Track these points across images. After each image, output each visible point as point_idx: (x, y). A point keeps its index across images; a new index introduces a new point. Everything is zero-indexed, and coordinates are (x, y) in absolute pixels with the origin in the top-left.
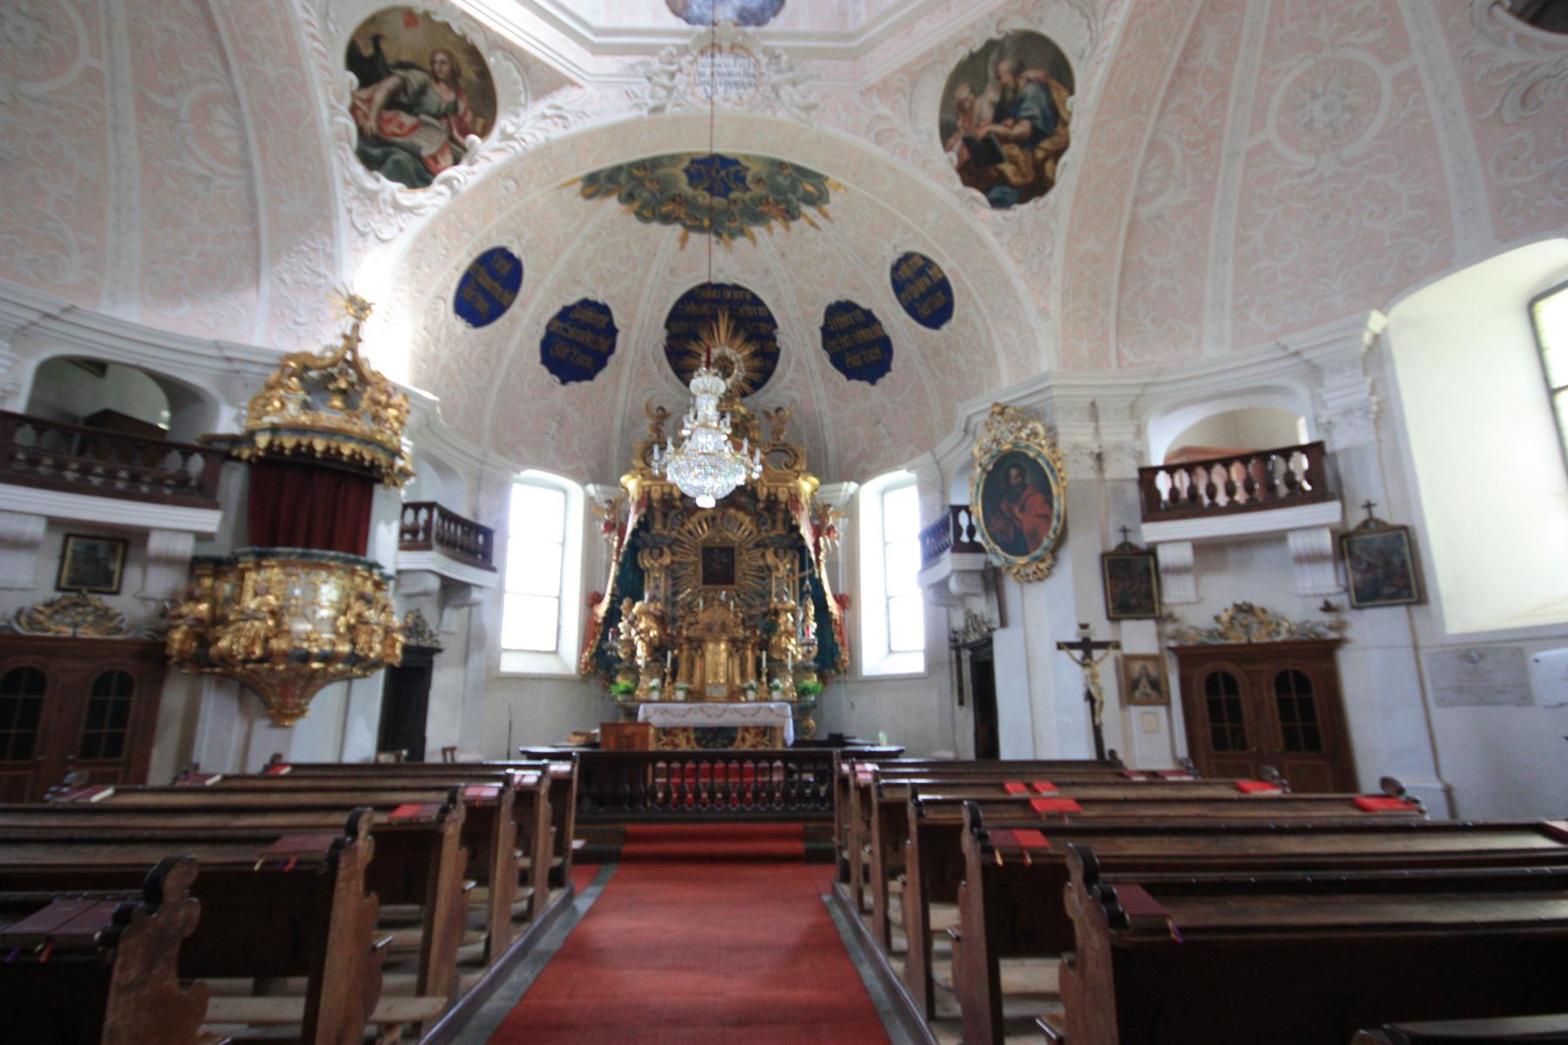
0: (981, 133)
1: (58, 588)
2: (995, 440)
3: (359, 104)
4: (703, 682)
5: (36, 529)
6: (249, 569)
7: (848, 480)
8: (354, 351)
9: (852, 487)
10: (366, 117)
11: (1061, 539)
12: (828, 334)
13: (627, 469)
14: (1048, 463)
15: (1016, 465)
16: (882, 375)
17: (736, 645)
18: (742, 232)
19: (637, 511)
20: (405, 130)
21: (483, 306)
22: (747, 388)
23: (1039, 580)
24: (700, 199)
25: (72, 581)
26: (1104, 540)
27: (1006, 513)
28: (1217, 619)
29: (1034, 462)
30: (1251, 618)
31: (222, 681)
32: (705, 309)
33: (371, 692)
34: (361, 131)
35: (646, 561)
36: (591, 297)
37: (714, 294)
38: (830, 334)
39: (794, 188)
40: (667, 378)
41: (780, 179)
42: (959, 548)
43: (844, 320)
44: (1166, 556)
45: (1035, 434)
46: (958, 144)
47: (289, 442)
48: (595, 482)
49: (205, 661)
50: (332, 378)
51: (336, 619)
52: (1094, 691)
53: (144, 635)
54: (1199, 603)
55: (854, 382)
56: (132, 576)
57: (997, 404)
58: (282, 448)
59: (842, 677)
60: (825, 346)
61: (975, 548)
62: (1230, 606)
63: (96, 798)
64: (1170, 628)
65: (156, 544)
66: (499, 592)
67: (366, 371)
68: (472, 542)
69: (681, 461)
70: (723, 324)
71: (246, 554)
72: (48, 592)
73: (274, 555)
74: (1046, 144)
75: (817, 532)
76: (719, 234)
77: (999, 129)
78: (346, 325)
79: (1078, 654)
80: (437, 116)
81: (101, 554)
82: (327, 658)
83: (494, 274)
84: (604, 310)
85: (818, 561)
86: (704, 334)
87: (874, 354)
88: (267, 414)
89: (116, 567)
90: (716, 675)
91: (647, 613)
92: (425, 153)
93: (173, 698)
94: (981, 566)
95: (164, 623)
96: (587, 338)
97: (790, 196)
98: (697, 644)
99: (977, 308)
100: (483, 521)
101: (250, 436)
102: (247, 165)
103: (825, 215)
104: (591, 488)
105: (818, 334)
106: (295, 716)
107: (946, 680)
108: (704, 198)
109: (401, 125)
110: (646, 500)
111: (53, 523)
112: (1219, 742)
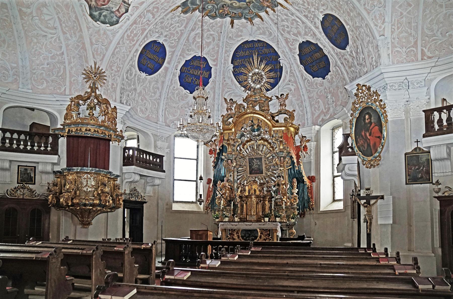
1: (18, 183)
15: (368, 113)
20: (106, 2)
22: (269, 87)
25: (21, 181)
43: (307, 50)
49: (58, 206)
63: (37, 244)
68: (154, 162)
70: (255, 57)
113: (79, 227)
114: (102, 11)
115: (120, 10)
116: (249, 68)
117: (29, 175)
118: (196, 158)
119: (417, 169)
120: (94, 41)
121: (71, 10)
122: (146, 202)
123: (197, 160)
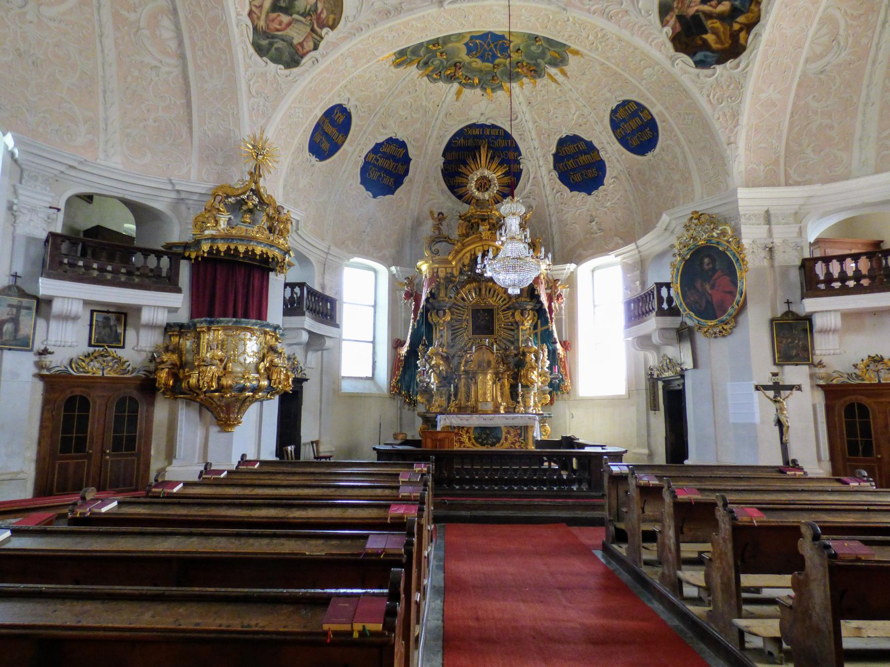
0: (691, 11)
1: (90, 345)
2: (693, 238)
3: (254, 9)
4: (477, 401)
5: (77, 308)
6: (203, 332)
7: (571, 263)
8: (256, 183)
9: (571, 267)
10: (259, 18)
11: (743, 308)
12: (558, 158)
13: (422, 257)
14: (734, 255)
15: (708, 256)
17: (498, 377)
18: (501, 87)
19: (429, 286)
20: (283, 26)
21: (325, 146)
23: (724, 336)
24: (474, 65)
25: (98, 341)
26: (774, 309)
27: (699, 287)
28: (855, 366)
29: (723, 254)
30: (880, 367)
31: (189, 401)
32: (470, 142)
33: (272, 406)
34: (255, 29)
35: (433, 318)
37: (477, 132)
39: (543, 55)
40: (443, 192)
41: (533, 48)
42: (661, 313)
43: (570, 149)
44: (819, 322)
45: (724, 233)
46: (672, 20)
47: (223, 247)
48: (396, 264)
50: (242, 202)
51: (257, 365)
52: (783, 419)
53: (142, 374)
55: (575, 193)
56: (131, 335)
57: (696, 212)
58: (218, 249)
59: (566, 396)
61: (674, 312)
62: (865, 357)
65: (146, 316)
66: (339, 340)
68: (324, 307)
69: (497, 265)
70: (483, 152)
71: (201, 323)
72: (83, 348)
73: (218, 322)
74: (741, 19)
75: (550, 299)
76: (484, 89)
77: (706, 8)
78: (250, 166)
79: (771, 394)
80: (304, 15)
81: (112, 323)
82: (255, 390)
83: (333, 123)
84: (403, 145)
85: (551, 319)
87: (592, 173)
88: (208, 228)
89: (120, 330)
90: (485, 394)
91: (437, 354)
92: (295, 42)
93: (161, 411)
94: (678, 326)
95: (152, 367)
96: (389, 164)
97: (539, 61)
98: (471, 376)
99: (678, 142)
100: (328, 293)
101: (197, 243)
102: (182, 57)
103: (564, 73)
104: (393, 269)
105: (551, 159)
106: (234, 425)
107: (643, 399)
108: (478, 63)
109: (281, 23)
110: (434, 276)
111: (86, 303)
112: (853, 449)
113: (214, 430)
114: (275, 40)
115: (305, 44)
116: (473, 166)
117: (114, 328)
119: (791, 343)
120: (254, 93)
121: (220, 30)
122: (306, 380)
123: (375, 306)
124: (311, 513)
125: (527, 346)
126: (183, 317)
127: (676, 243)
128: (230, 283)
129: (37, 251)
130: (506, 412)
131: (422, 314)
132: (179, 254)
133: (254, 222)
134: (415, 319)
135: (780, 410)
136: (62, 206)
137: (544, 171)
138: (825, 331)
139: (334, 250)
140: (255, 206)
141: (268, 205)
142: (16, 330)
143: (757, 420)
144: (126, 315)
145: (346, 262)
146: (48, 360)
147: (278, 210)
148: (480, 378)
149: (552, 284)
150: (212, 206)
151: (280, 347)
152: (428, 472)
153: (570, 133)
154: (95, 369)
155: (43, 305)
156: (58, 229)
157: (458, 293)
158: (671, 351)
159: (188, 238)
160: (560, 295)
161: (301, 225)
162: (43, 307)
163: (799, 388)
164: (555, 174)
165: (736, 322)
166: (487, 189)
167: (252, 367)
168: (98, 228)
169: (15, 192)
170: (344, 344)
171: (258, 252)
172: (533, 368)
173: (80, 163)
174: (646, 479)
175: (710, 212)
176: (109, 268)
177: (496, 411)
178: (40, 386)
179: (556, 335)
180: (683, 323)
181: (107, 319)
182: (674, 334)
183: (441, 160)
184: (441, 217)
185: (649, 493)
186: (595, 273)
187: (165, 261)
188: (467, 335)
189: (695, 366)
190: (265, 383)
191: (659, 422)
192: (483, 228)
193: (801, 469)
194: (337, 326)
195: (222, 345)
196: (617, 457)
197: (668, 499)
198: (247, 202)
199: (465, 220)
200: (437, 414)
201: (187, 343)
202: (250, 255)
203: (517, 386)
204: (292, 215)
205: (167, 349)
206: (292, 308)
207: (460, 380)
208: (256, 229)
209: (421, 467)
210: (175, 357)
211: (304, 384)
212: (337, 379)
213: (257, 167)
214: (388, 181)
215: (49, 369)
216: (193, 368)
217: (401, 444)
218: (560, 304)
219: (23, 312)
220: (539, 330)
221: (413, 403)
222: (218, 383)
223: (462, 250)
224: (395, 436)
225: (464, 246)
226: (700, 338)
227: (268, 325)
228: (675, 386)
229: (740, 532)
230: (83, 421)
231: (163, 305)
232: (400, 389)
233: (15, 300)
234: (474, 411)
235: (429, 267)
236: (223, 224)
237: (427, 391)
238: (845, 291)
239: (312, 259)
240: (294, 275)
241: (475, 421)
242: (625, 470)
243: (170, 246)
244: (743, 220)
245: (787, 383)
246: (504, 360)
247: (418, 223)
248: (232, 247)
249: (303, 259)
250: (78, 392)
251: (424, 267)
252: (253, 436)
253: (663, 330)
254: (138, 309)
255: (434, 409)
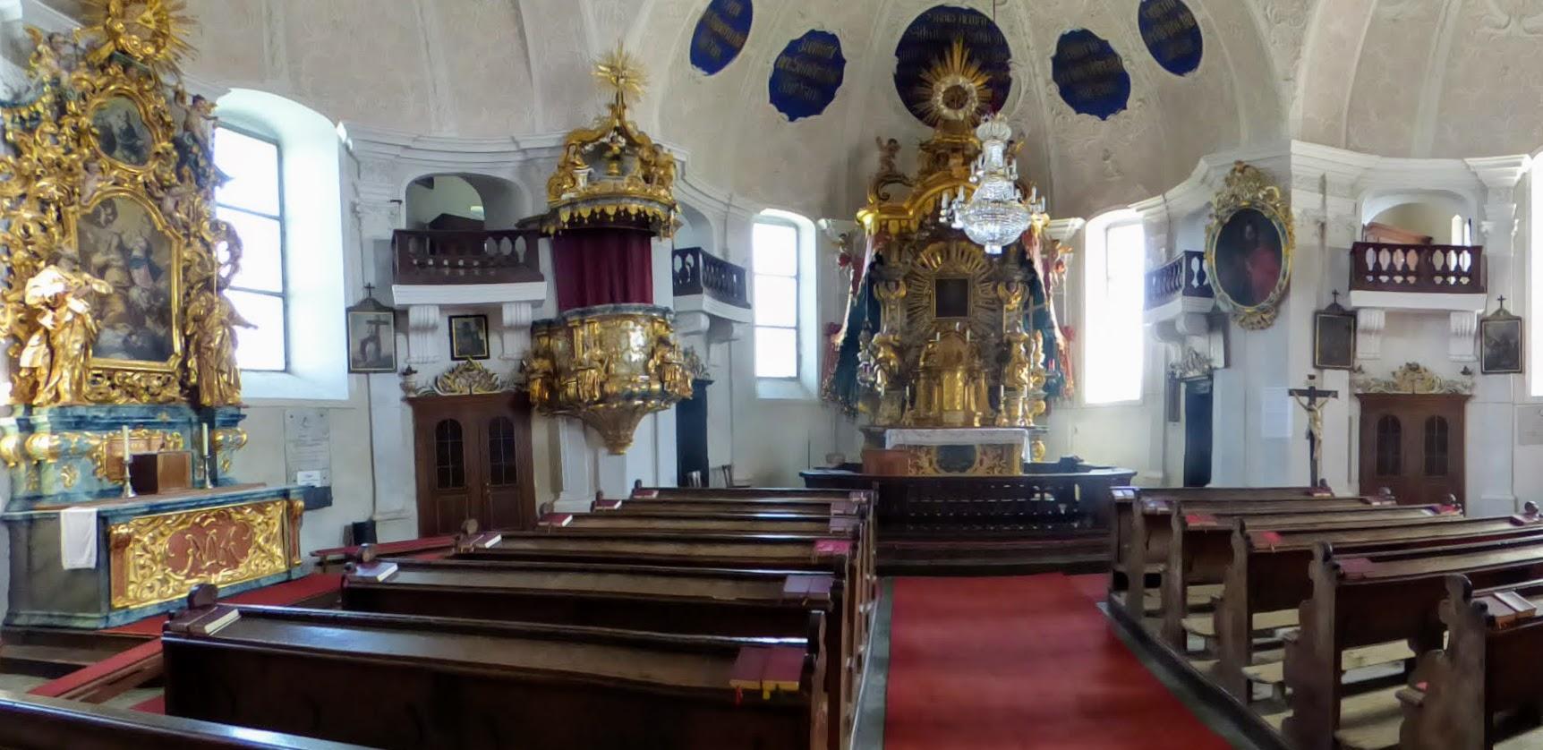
1: (453, 358)
4: (941, 409)
5: (434, 316)
8: (620, 117)
9: (1076, 223)
11: (1285, 293)
13: (863, 204)
16: (1113, 111)
17: (971, 376)
25: (460, 352)
29: (1268, 222)
33: (669, 417)
35: (880, 292)
36: (818, 28)
38: (1061, 65)
42: (1189, 291)
43: (1076, 50)
44: (1363, 319)
45: (1270, 195)
47: (585, 212)
50: (606, 147)
51: (646, 363)
52: (1316, 432)
53: (512, 388)
54: (1380, 358)
56: (494, 341)
57: (1239, 162)
60: (1056, 77)
61: (1206, 292)
64: (1360, 378)
65: (508, 316)
66: (751, 326)
67: (635, 134)
75: (1047, 269)
79: (1305, 400)
82: (646, 396)
84: (832, 40)
86: (935, 62)
88: (564, 191)
89: (482, 336)
90: (953, 400)
91: (885, 343)
93: (539, 432)
94: (1208, 309)
95: (522, 378)
96: (812, 70)
98: (934, 375)
101: (555, 212)
104: (823, 222)
105: (1050, 64)
106: (624, 445)
107: (1160, 406)
111: (443, 308)
113: (603, 452)
118: (279, 290)
123: (798, 277)
124: (720, 551)
125: (1014, 333)
126: (550, 311)
127: (1214, 200)
128: (603, 255)
129: (387, 254)
130: (983, 426)
131: (864, 287)
132: (535, 231)
133: (623, 172)
134: (854, 293)
135: (1314, 420)
136: (403, 197)
137: (1040, 80)
138: (1368, 331)
139: (738, 201)
140: (622, 149)
141: (640, 146)
142: (378, 349)
143: (1290, 435)
144: (485, 317)
145: (756, 216)
146: (414, 378)
147: (655, 150)
148: (946, 377)
149: (1050, 246)
150: (566, 161)
151: (671, 337)
152: (869, 502)
153: (1077, 27)
154: (461, 387)
155: (400, 316)
156: (403, 226)
157: (916, 257)
158: (1199, 343)
159: (543, 209)
160: (1060, 263)
161: (688, 166)
162: (401, 319)
163: (1335, 394)
164: (1054, 88)
165: (1277, 312)
166: (962, 106)
167: (640, 366)
168: (444, 216)
169: (357, 193)
170: (759, 333)
171: (633, 211)
172: (1022, 364)
173: (415, 140)
174: (1154, 505)
175: (1256, 165)
176: (461, 263)
177: (968, 423)
178: (409, 410)
179: (1054, 318)
180: (1216, 308)
181: (466, 325)
182: (1203, 322)
183: (894, 62)
184: (892, 147)
185: (1157, 522)
186: (1111, 232)
187: (521, 243)
188: (928, 317)
189: (1227, 364)
190: (656, 387)
191: (1178, 436)
192: (955, 162)
193: (1328, 490)
194: (748, 306)
195: (600, 341)
196: (1124, 480)
197: (1176, 527)
198: (611, 146)
199: (927, 150)
200: (886, 427)
201: (559, 345)
202: (623, 216)
203: (998, 389)
204: (676, 156)
205: (536, 355)
206: (685, 283)
207: (918, 379)
208: (626, 180)
209: (859, 497)
210: (546, 364)
211: (709, 388)
212: (750, 380)
213: (619, 96)
214: (812, 95)
215: (416, 391)
216: (570, 374)
217: (838, 468)
218: (1060, 275)
219: (382, 327)
220: (1032, 308)
221: (853, 413)
222: (602, 391)
223: (921, 194)
224: (829, 458)
225: (926, 188)
226: (1234, 327)
227: (655, 309)
228: (1202, 389)
229: (1257, 560)
230: (458, 447)
231: (524, 299)
232: (835, 393)
233: (372, 315)
234: (938, 423)
235: (874, 219)
236: (582, 182)
237: (871, 394)
238: (1391, 287)
239: (708, 214)
240: (684, 237)
241: (938, 437)
242: (1130, 494)
243: (523, 223)
244: (1294, 183)
245: (1326, 388)
246: (979, 352)
247: (857, 156)
248: (597, 210)
249: (694, 216)
250: (447, 415)
251: (867, 218)
252: (649, 457)
253: (1191, 316)
254: (497, 308)
255: (882, 421)
